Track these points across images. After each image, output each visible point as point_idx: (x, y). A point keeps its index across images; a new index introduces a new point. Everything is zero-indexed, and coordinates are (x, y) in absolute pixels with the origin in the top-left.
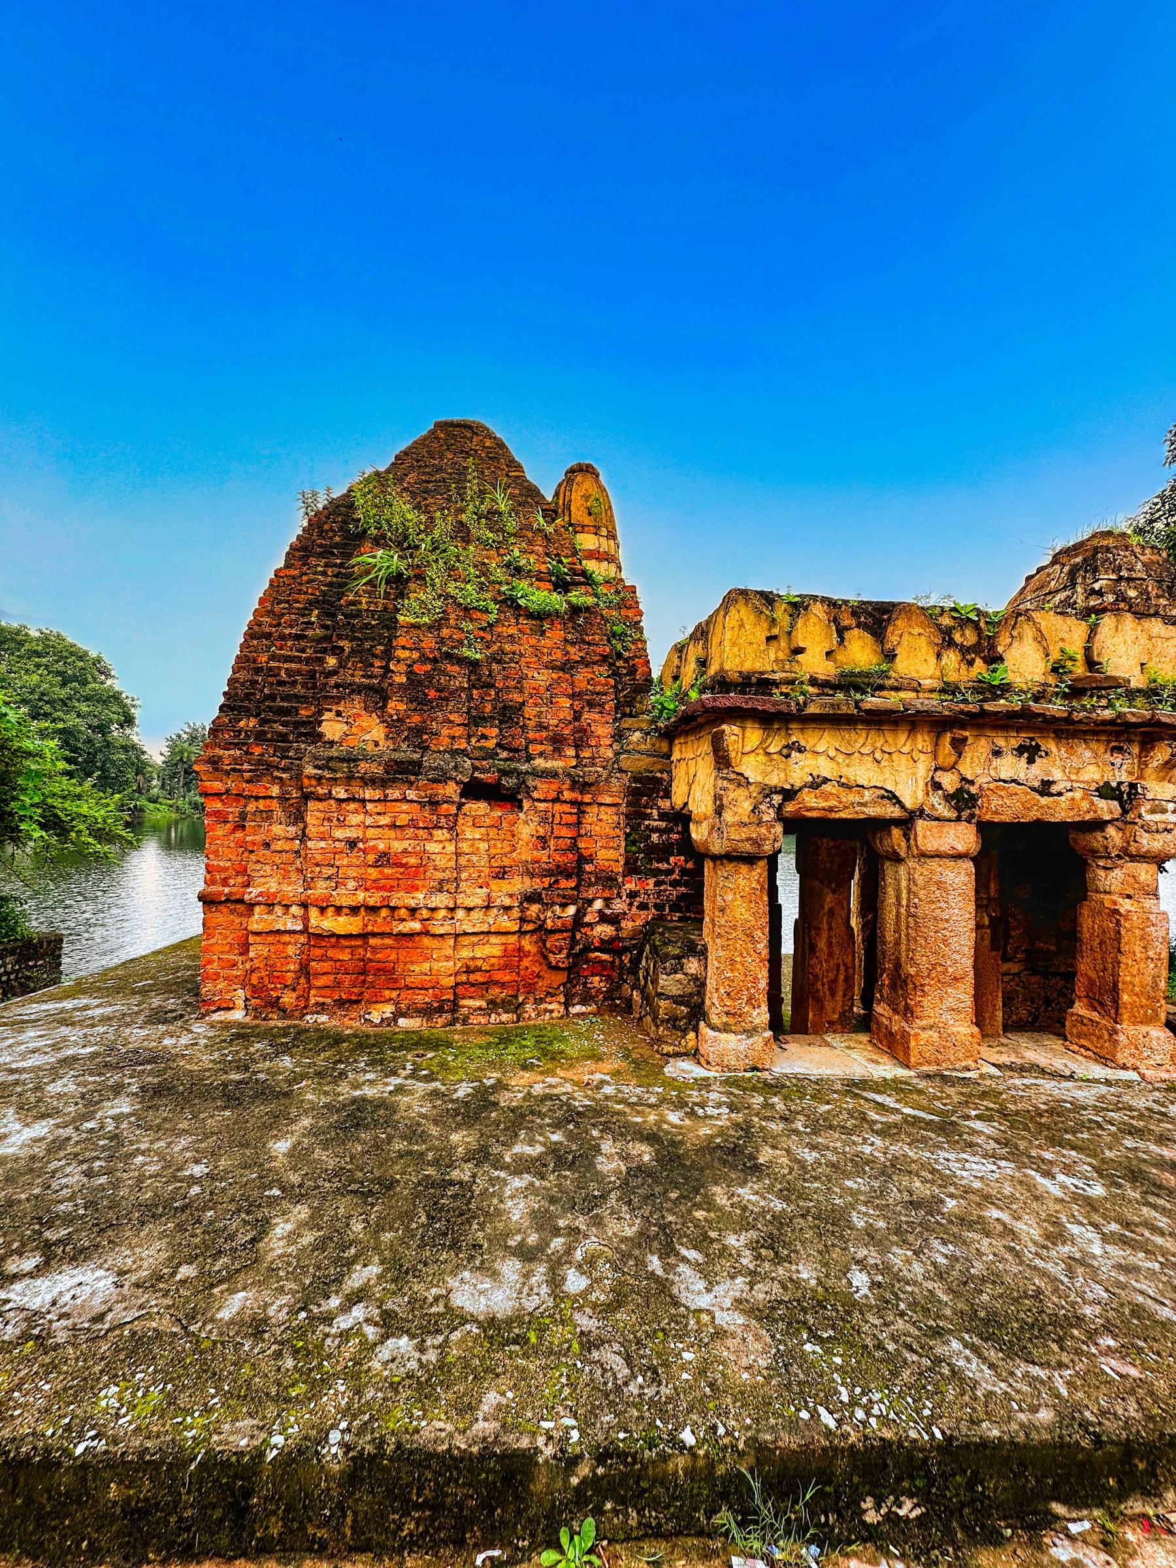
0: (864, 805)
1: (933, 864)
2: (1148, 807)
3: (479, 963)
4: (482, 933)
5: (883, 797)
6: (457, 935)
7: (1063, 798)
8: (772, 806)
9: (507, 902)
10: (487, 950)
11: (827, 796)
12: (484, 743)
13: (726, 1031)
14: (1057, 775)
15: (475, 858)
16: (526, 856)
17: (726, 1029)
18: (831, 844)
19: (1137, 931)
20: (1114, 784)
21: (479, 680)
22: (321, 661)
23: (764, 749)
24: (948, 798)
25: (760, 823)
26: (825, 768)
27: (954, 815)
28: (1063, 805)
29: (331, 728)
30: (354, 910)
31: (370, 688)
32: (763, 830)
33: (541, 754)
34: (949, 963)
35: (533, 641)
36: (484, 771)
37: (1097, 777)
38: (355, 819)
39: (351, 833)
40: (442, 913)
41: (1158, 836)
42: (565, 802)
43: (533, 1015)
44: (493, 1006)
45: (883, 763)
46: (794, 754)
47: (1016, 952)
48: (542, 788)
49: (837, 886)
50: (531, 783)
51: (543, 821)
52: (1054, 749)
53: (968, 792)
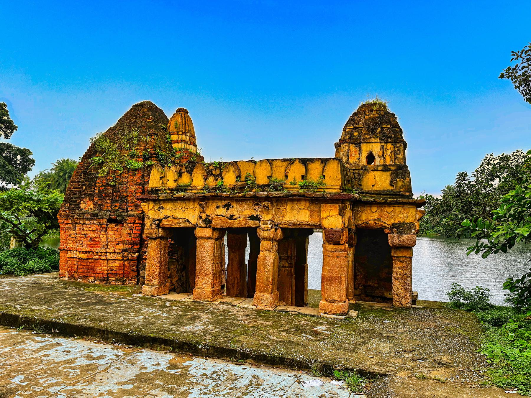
1: (202, 240)
6: (108, 260)
9: (119, 251)
10: (114, 265)
11: (169, 221)
12: (116, 208)
14: (235, 213)
16: (125, 239)
17: (147, 285)
20: (255, 216)
22: (82, 188)
24: (203, 221)
26: (168, 213)
29: (82, 206)
31: (91, 194)
33: (131, 210)
35: (132, 177)
36: (113, 216)
37: (249, 213)
38: (85, 229)
39: (85, 233)
40: (103, 254)
47: (359, 286)
48: (129, 220)
50: (126, 218)
51: (130, 229)
52: (235, 205)
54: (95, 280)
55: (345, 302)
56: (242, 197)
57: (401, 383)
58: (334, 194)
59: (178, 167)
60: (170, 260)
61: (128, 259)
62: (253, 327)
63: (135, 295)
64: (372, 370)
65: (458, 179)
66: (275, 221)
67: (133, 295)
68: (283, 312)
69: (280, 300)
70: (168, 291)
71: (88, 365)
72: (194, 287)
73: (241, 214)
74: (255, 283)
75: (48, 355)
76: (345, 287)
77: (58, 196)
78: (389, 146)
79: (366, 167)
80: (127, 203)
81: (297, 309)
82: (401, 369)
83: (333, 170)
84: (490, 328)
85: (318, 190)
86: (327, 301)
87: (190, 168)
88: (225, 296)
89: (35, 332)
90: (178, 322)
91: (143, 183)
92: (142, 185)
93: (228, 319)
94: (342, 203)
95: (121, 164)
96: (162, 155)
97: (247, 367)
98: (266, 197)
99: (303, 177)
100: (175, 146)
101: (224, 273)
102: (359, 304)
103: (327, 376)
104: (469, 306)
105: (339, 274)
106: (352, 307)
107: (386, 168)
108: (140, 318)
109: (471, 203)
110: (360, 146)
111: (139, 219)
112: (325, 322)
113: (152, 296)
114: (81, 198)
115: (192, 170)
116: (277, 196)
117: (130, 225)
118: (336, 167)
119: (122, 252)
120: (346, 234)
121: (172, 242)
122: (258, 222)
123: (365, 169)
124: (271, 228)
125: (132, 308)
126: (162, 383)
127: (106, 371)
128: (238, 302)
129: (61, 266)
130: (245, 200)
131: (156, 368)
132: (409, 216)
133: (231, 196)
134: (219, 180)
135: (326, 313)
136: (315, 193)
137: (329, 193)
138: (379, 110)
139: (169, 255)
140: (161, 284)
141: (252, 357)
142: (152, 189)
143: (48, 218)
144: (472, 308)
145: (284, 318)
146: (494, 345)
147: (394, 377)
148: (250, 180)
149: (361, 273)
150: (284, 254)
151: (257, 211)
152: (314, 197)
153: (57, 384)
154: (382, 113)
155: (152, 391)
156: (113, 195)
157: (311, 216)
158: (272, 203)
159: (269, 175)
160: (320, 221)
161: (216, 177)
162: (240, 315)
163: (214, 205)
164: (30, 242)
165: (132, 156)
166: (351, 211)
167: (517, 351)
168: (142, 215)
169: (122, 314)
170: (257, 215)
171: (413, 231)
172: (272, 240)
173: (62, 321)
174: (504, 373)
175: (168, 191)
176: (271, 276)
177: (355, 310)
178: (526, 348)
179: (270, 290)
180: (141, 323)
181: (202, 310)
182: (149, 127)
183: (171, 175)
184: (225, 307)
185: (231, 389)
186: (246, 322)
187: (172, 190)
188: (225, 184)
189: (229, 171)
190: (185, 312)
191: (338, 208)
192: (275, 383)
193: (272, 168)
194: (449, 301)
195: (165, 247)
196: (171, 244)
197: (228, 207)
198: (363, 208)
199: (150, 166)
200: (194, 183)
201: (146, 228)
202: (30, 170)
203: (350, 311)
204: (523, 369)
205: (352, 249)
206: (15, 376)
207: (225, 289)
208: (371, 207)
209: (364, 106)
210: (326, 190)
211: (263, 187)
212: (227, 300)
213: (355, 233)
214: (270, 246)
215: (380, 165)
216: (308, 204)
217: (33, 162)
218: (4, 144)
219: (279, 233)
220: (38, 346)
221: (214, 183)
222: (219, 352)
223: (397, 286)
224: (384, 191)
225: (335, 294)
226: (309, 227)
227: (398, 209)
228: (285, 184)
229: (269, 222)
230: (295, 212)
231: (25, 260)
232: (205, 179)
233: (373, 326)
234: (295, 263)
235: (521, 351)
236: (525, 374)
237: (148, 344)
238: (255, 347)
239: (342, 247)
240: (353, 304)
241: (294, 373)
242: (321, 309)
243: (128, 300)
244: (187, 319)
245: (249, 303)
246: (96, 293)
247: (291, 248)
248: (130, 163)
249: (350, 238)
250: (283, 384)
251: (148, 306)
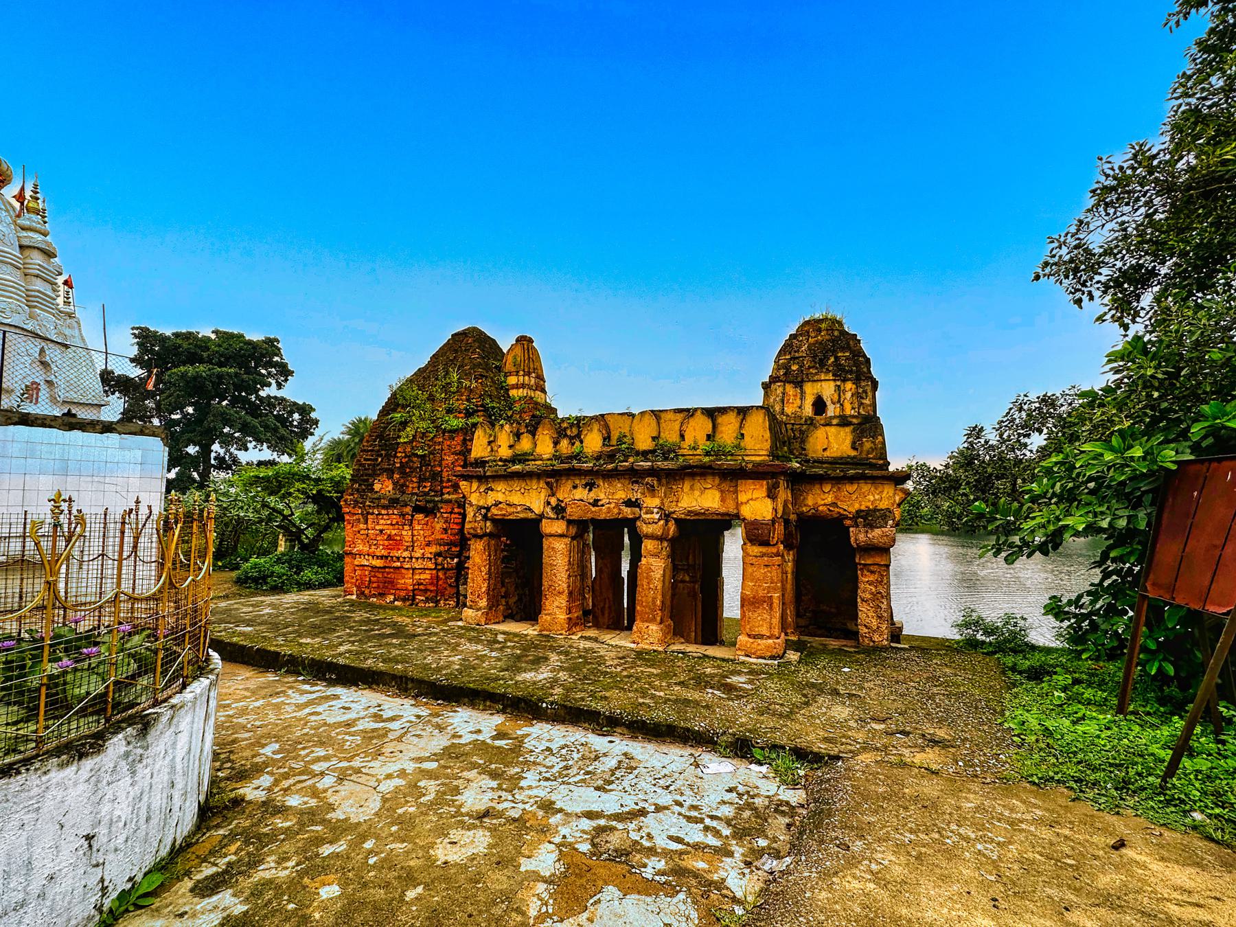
1: (551, 539)
11: (501, 509)
14: (602, 496)
17: (471, 607)
24: (553, 509)
26: (500, 497)
29: (377, 487)
30: (382, 557)
38: (382, 522)
44: (427, 600)
51: (446, 522)
54: (395, 600)
56: (612, 470)
57: (864, 772)
58: (759, 464)
61: (443, 568)
62: (629, 677)
64: (816, 750)
65: (969, 436)
69: (675, 634)
71: (373, 730)
73: (610, 498)
75: (318, 714)
77: (344, 471)
78: (849, 385)
80: (442, 482)
82: (865, 749)
84: (1022, 684)
86: (749, 636)
89: (301, 678)
90: (514, 665)
92: (464, 455)
96: (493, 408)
97: (617, 739)
99: (709, 437)
100: (513, 393)
103: (742, 757)
104: (993, 650)
106: (789, 645)
107: (844, 422)
109: (991, 475)
110: (801, 387)
114: (375, 475)
115: (536, 429)
116: (669, 470)
118: (761, 420)
120: (780, 529)
126: (481, 762)
127: (399, 739)
128: (609, 636)
129: (346, 579)
131: (475, 736)
132: (883, 497)
134: (578, 443)
135: (747, 656)
138: (830, 330)
140: (491, 607)
141: (624, 724)
142: (476, 459)
143: (329, 506)
144: (1000, 648)
146: (1028, 712)
147: (852, 762)
153: (326, 758)
154: (836, 333)
155: (465, 774)
157: (723, 500)
158: (659, 480)
162: (610, 656)
163: (569, 484)
164: (306, 541)
167: (1067, 723)
171: (891, 522)
172: (660, 539)
173: (341, 661)
174: (1043, 760)
176: (660, 597)
177: (796, 650)
178: (1083, 718)
181: (552, 649)
182: (475, 366)
184: (588, 644)
185: (588, 773)
186: (619, 669)
190: (524, 650)
192: (658, 765)
194: (958, 637)
196: (506, 545)
199: (475, 425)
200: (539, 450)
202: (312, 434)
204: (1075, 753)
206: (266, 745)
209: (807, 323)
211: (645, 454)
212: (592, 633)
215: (835, 417)
217: (316, 422)
218: (275, 398)
219: (672, 527)
220: (304, 699)
222: (572, 715)
223: (866, 614)
224: (842, 458)
227: (866, 487)
230: (697, 493)
231: (300, 570)
232: (556, 443)
233: (824, 677)
235: (1074, 723)
236: (1079, 763)
237: (466, 700)
238: (629, 709)
239: (774, 550)
241: (690, 750)
243: (442, 630)
246: (396, 619)
250: (673, 767)
251: (470, 640)
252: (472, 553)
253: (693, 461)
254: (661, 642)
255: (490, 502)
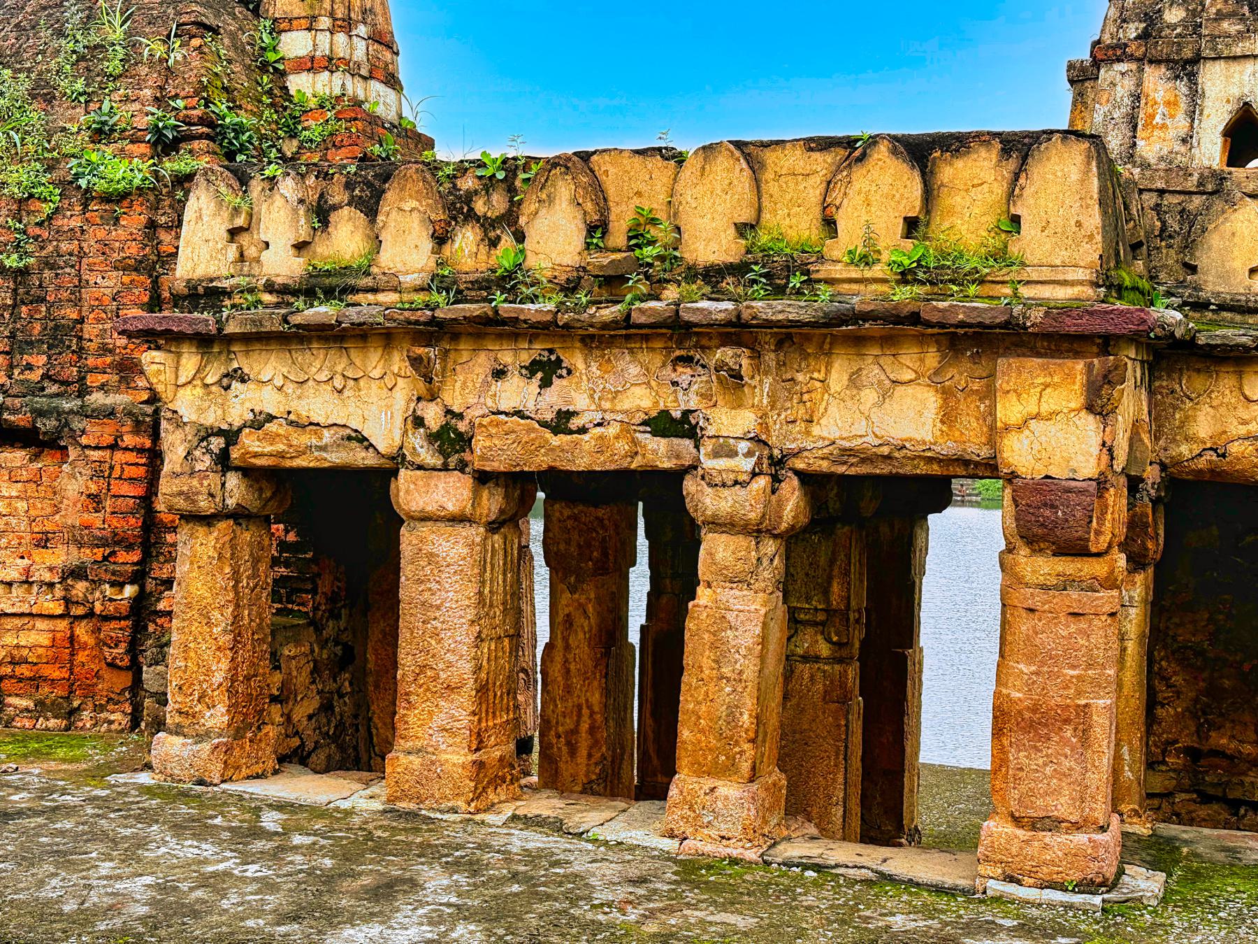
0: (323, 448)
1: (424, 529)
2: (710, 448)
3: (25, 652)
4: (22, 615)
5: (349, 438)
7: (586, 437)
8: (209, 451)
9: (47, 577)
10: (26, 639)
11: (273, 438)
13: (177, 734)
14: (580, 401)
15: (14, 521)
16: (74, 519)
17: (178, 731)
18: (567, 512)
19: (706, 636)
20: (677, 414)
21: (27, 293)
23: (202, 380)
24: (432, 438)
25: (192, 474)
26: (269, 401)
27: (439, 462)
28: (587, 447)
32: (195, 482)
33: (102, 387)
34: (441, 666)
35: (101, 234)
36: (15, 411)
37: (646, 403)
41: (725, 492)
42: (126, 449)
43: (88, 725)
44: (41, 708)
45: (346, 393)
46: (235, 385)
48: (96, 432)
49: (577, 580)
50: (77, 424)
51: (97, 475)
52: (580, 365)
53: (456, 431)
55: (1103, 829)
58: (1065, 310)
59: (311, 180)
60: (279, 619)
61: (90, 614)
63: (122, 778)
66: (773, 441)
67: (112, 779)
68: (806, 867)
70: (271, 763)
72: (388, 745)
73: (610, 407)
74: (674, 733)
76: (1106, 761)
79: (1221, 178)
80: (80, 351)
81: (874, 857)
83: (1062, 198)
85: (987, 290)
86: (1017, 821)
87: (369, 184)
88: (534, 789)
91: (154, 264)
92: (150, 270)
93: (549, 897)
94: (1105, 351)
95: (49, 169)
96: (239, 129)
98: (729, 323)
99: (912, 226)
101: (530, 683)
102: (1170, 840)
105: (1079, 694)
106: (1137, 850)
108: (139, 885)
111: (138, 427)
112: (1008, 923)
113: (201, 782)
115: (378, 195)
116: (777, 319)
117: (95, 455)
118: (1075, 176)
119: (63, 579)
120: (1117, 500)
121: (291, 537)
122: (688, 443)
123: (1215, 188)
124: (754, 474)
125: (96, 836)
130: (628, 338)
133: (564, 318)
134: (507, 241)
135: (1011, 879)
136: (970, 304)
137: (1039, 302)
139: (275, 596)
140: (245, 722)
142: (192, 285)
145: (809, 900)
148: (651, 243)
149: (1178, 694)
150: (808, 599)
151: (687, 392)
152: (962, 324)
156: (16, 317)
157: (948, 417)
158: (756, 356)
159: (746, 216)
160: (992, 442)
161: (490, 229)
162: (604, 878)
163: (482, 364)
165: (99, 131)
166: (1144, 395)
168: (149, 409)
169: (57, 865)
170: (686, 413)
172: (757, 531)
175: (267, 298)
176: (749, 702)
177: (1154, 865)
179: (745, 767)
180: (143, 910)
181: (429, 852)
183: (279, 217)
184: (537, 840)
186: (633, 915)
187: (284, 291)
188: (532, 261)
189: (551, 200)
191: (1080, 379)
193: (757, 183)
195: (256, 561)
197: (546, 371)
198: (1199, 382)
200: (389, 258)
201: (167, 468)
203: (1129, 869)
205: (1139, 578)
207: (535, 756)
208: (1240, 374)
210: (1025, 292)
211: (712, 276)
212: (545, 805)
213: (1155, 502)
214: (746, 560)
216: (932, 358)
219: (793, 503)
221: (482, 256)
225: (1057, 792)
226: (935, 469)
228: (821, 258)
229: (743, 446)
230: (869, 396)
232: (441, 239)
234: (862, 643)
239: (1098, 568)
240: (1139, 839)
242: (987, 859)
244: (355, 895)
245: (644, 822)
247: (847, 573)
248: (93, 168)
249: (1135, 525)
251: (178, 829)
252: (182, 569)
253: (861, 298)
254: (751, 834)
255: (237, 414)
